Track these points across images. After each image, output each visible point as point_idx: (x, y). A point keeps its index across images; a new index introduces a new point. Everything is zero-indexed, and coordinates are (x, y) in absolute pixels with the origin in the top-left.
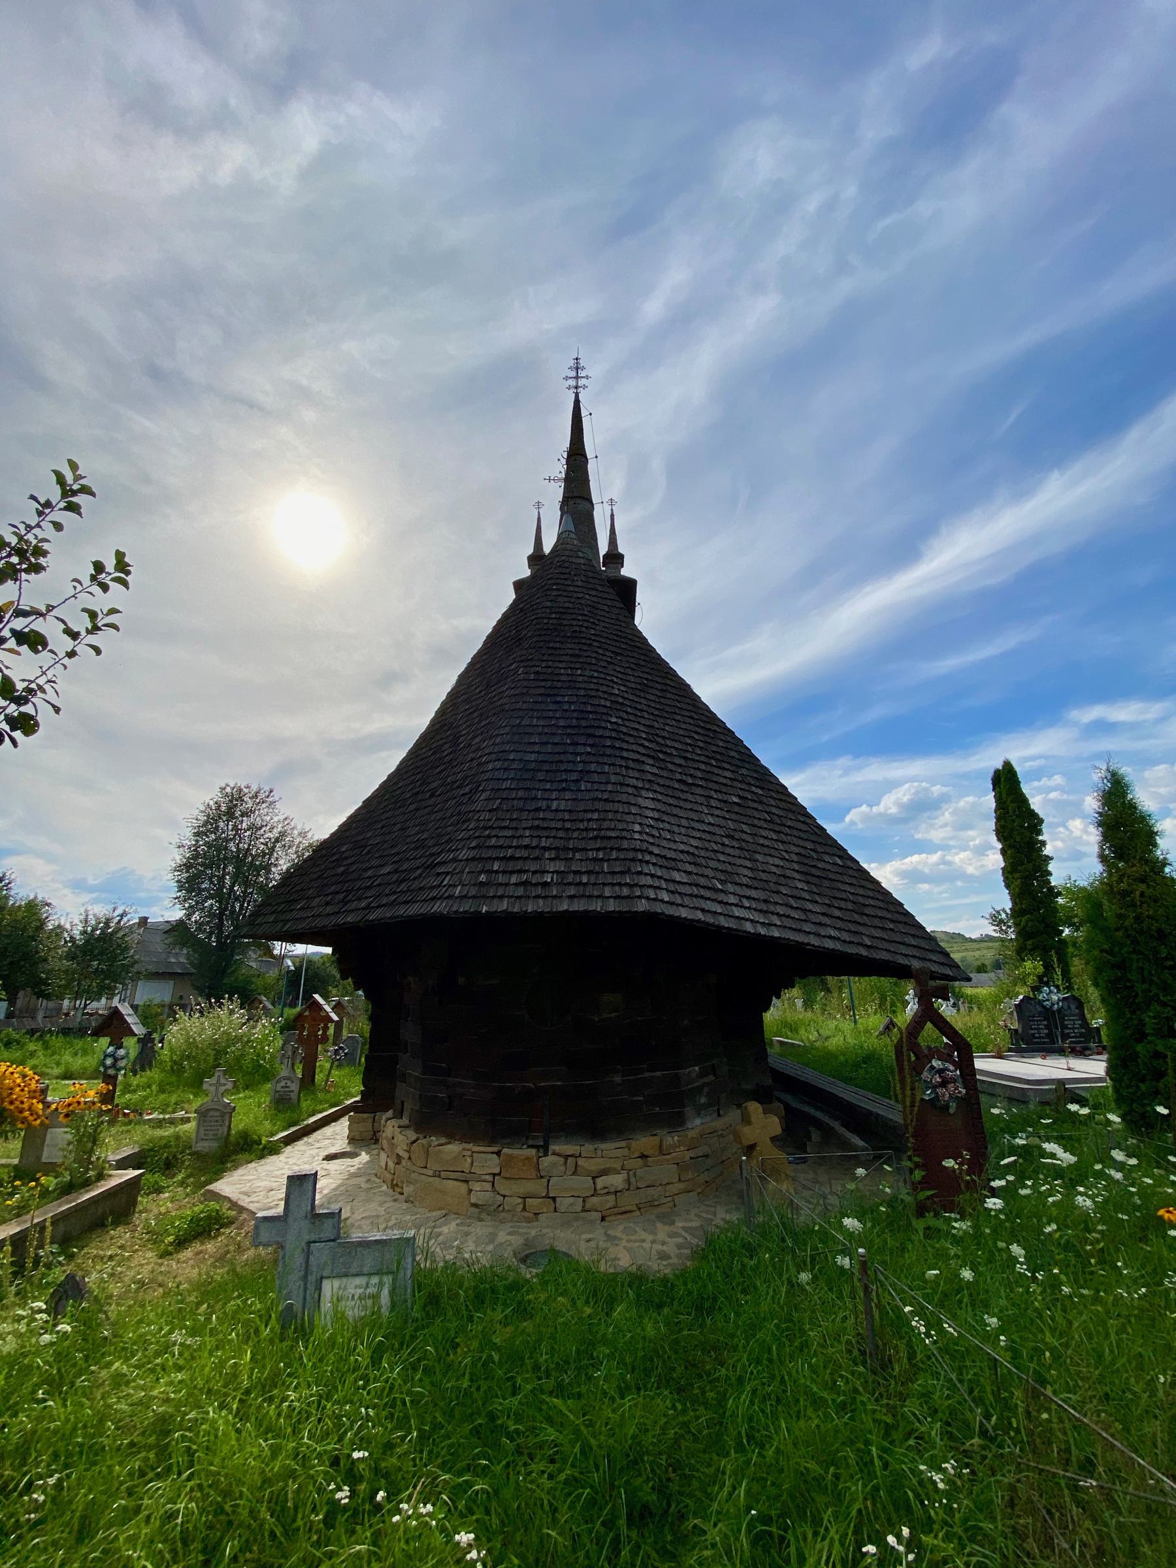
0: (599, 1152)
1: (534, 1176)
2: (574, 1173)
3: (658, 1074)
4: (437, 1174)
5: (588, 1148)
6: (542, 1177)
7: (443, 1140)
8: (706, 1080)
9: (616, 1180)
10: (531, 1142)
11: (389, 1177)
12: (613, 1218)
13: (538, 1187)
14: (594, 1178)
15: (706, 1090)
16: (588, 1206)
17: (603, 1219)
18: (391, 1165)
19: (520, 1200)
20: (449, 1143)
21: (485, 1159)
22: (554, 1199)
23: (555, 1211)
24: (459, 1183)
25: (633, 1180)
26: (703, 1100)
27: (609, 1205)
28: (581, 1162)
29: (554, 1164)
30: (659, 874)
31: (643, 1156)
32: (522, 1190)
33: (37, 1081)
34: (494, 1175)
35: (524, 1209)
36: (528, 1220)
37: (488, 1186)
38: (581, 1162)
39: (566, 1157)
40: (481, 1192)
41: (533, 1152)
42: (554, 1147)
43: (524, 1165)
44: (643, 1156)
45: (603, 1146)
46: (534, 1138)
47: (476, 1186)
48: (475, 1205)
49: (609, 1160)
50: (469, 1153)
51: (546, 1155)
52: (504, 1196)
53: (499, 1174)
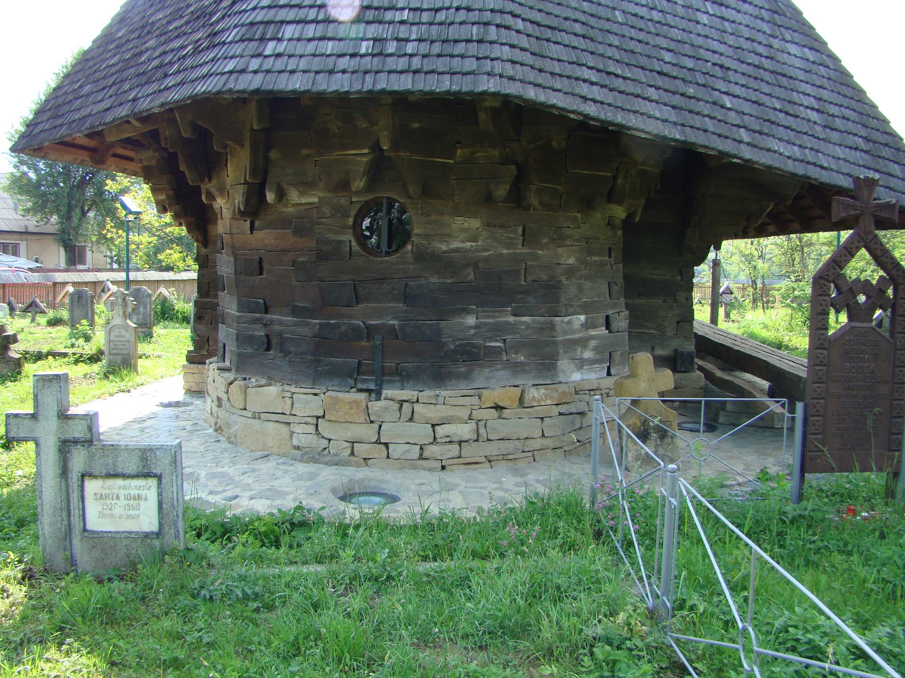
0: (441, 400)
1: (362, 420)
2: (411, 419)
3: (526, 319)
4: (256, 416)
5: (427, 394)
6: (372, 422)
7: (264, 381)
8: (592, 332)
9: (464, 431)
10: (360, 386)
11: (213, 421)
12: (455, 467)
13: (370, 433)
14: (433, 426)
15: (593, 343)
16: (425, 454)
17: (443, 468)
18: (215, 409)
19: (348, 444)
20: (270, 385)
21: (307, 401)
22: (386, 445)
23: (388, 457)
24: (283, 426)
25: (482, 431)
26: (588, 355)
27: (450, 455)
28: (417, 407)
29: (386, 408)
30: (511, 73)
31: (498, 407)
32: (349, 435)
33: (806, 509)
34: (318, 418)
35: (352, 453)
36: (358, 465)
37: (312, 429)
38: (417, 407)
39: (401, 402)
40: (304, 436)
41: (363, 396)
42: (386, 392)
43: (351, 408)
44: (498, 407)
45: (444, 393)
46: (365, 381)
47: (298, 429)
48: (298, 448)
49: (448, 407)
50: (289, 394)
51: (378, 399)
52: (330, 440)
53: (324, 416)
